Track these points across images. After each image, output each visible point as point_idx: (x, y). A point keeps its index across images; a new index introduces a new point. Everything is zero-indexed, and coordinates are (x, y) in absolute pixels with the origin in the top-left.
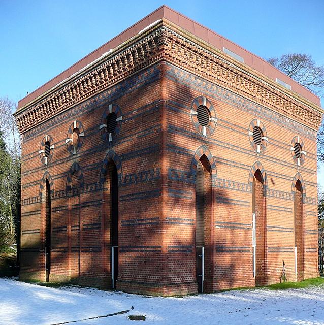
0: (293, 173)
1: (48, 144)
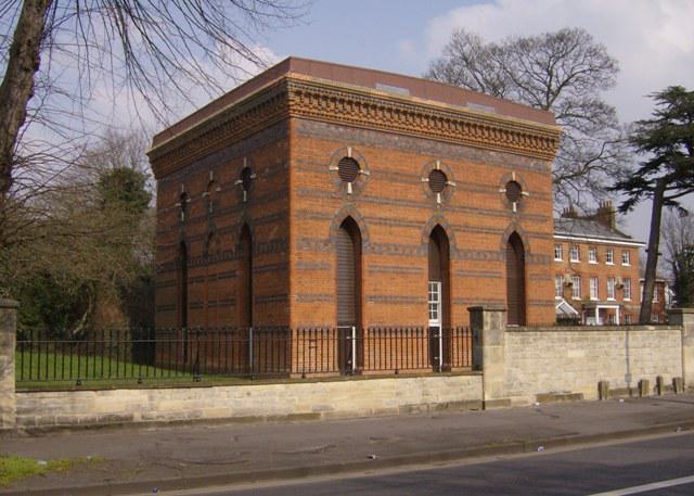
0: (504, 224)
1: (183, 196)
